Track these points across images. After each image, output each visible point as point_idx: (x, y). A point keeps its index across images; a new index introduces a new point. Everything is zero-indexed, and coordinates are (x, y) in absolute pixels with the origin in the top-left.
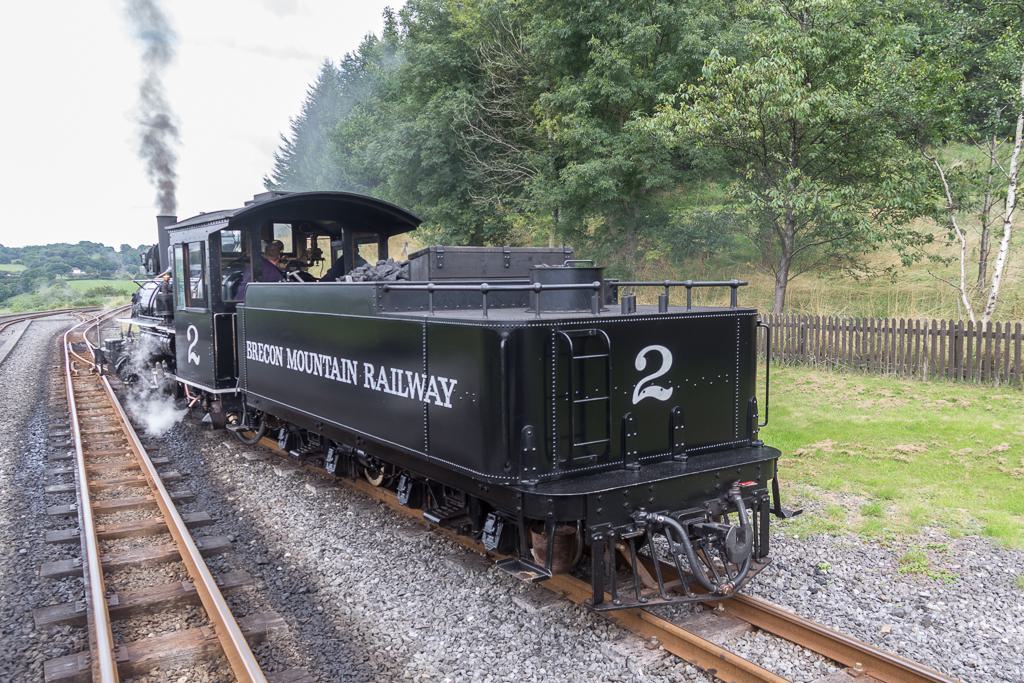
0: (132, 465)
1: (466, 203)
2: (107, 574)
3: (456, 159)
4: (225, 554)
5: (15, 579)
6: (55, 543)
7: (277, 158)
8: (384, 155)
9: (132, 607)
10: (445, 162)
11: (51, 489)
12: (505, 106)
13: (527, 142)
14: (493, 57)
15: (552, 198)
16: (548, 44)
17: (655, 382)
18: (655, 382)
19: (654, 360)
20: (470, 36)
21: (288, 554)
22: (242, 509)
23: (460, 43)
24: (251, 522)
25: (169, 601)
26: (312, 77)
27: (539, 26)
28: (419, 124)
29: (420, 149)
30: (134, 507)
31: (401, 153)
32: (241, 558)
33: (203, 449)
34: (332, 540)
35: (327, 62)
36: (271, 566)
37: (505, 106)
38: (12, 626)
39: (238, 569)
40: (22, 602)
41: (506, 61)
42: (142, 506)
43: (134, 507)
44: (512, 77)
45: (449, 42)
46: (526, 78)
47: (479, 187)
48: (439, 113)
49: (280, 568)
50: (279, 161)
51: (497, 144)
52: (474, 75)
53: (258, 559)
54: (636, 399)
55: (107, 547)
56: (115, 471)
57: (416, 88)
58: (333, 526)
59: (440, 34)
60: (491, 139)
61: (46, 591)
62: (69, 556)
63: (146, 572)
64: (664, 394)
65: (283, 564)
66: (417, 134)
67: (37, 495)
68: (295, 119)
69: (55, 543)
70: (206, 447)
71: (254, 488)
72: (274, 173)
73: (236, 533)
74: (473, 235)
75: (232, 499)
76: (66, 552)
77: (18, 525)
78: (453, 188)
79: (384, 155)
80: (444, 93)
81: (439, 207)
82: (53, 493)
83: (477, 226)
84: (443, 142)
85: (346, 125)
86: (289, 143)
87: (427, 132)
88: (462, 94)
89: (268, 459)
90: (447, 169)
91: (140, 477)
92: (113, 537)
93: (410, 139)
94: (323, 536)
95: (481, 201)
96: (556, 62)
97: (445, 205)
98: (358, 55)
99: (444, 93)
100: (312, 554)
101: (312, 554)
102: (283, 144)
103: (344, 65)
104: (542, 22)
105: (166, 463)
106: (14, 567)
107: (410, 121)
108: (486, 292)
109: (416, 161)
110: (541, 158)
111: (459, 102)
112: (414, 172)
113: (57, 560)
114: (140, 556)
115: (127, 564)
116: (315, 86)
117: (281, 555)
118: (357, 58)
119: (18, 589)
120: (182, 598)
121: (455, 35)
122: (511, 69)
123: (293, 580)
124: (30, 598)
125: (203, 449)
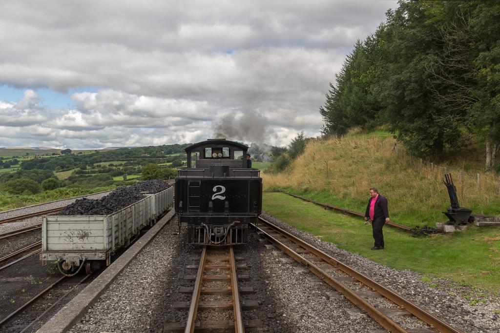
0: (226, 259)
1: (431, 121)
2: (200, 311)
3: (426, 95)
4: (254, 310)
5: (162, 307)
6: (183, 293)
7: (328, 97)
8: (382, 94)
9: (205, 329)
10: (419, 97)
11: (189, 267)
12: (459, 62)
13: (472, 83)
14: (450, 34)
15: (485, 117)
16: (486, 22)
17: (220, 195)
18: (220, 195)
19: (219, 190)
20: (437, 22)
21: (284, 315)
22: (270, 288)
23: (431, 26)
24: (272, 295)
25: (222, 329)
26: (350, 52)
27: (481, 11)
28: (404, 75)
29: (404, 90)
30: (221, 280)
31: (393, 92)
32: (261, 313)
33: (261, 255)
34: (310, 310)
35: (359, 42)
36: (275, 320)
37: (459, 62)
38: (155, 329)
39: (258, 318)
40: (162, 318)
41: (459, 35)
42: (225, 280)
43: (221, 280)
44: (463, 44)
45: (425, 26)
46: (471, 44)
47: (440, 112)
48: (416, 69)
49: (278, 322)
50: (329, 98)
51: (452, 85)
52: (440, 45)
53: (269, 315)
54: (213, 198)
55: (204, 298)
56: (218, 261)
57: (404, 55)
58: (313, 304)
59: (420, 22)
60: (449, 82)
61: (173, 315)
62: (187, 300)
63: (217, 313)
64: (223, 198)
65: (281, 320)
66: (403, 81)
67: (182, 269)
68: (339, 75)
69: (183, 293)
70: (263, 254)
71: (280, 278)
72: (325, 105)
73: (263, 300)
74: (436, 140)
75: (268, 282)
76: (186, 298)
77: (170, 282)
78: (424, 111)
79: (382, 94)
80: (420, 57)
81: (415, 124)
82: (189, 269)
83: (439, 134)
84: (419, 86)
85: (366, 77)
86: (335, 89)
87: (409, 81)
88: (431, 57)
89: (291, 263)
90: (421, 101)
91: (228, 266)
92: (208, 294)
93: (399, 85)
94: (305, 308)
95: (442, 119)
96: (492, 32)
97: (418, 123)
98: (374, 37)
99: (420, 57)
100: (297, 317)
101: (297, 317)
102: (332, 89)
103: (367, 44)
104: (483, 9)
105: (242, 260)
106: (163, 302)
107: (399, 74)
108: (251, 172)
109: (401, 97)
110: (480, 93)
111: (429, 62)
112: (400, 103)
113: (181, 301)
114: (216, 305)
115: (209, 308)
116: (351, 56)
117: (282, 315)
118: (374, 39)
119: (162, 312)
120: (228, 329)
121: (428, 22)
122: (463, 39)
123: (283, 329)
124: (166, 317)
125: (261, 255)
